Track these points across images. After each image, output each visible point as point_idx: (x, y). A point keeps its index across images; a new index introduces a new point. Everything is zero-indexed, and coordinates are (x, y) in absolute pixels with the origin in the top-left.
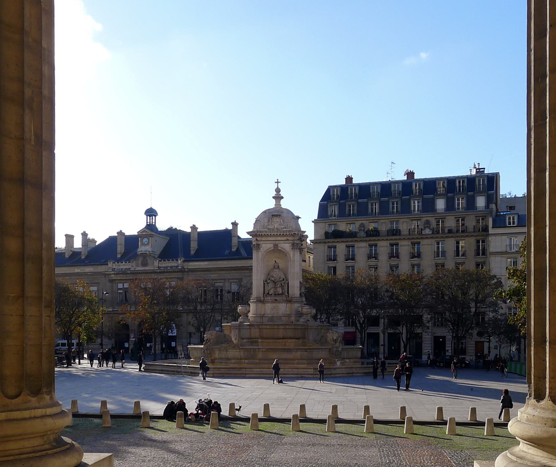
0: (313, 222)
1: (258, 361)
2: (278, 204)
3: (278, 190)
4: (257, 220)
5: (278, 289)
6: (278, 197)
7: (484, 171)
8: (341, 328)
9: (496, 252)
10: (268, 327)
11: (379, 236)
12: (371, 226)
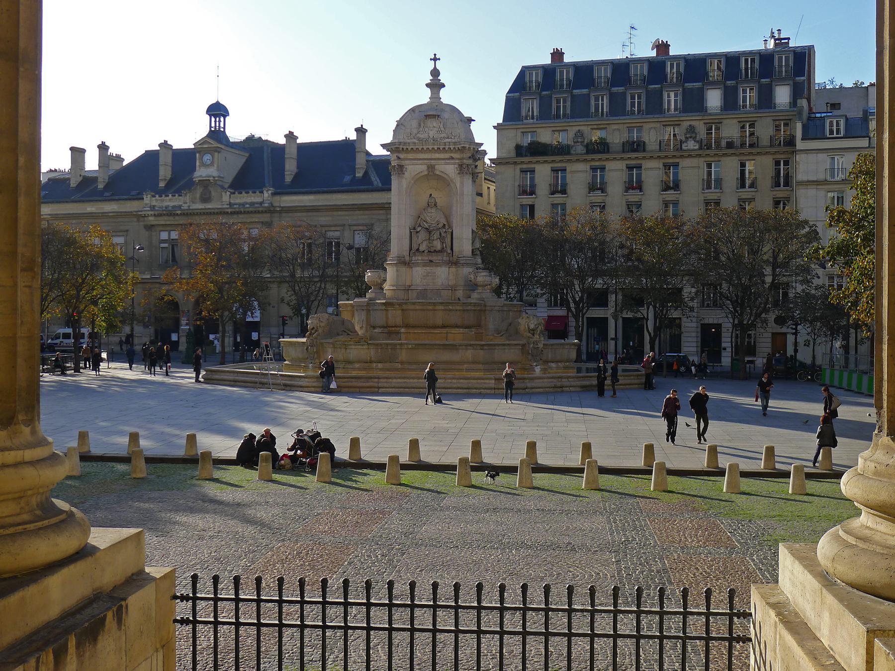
2: (435, 96)
3: (435, 73)
4: (400, 124)
5: (435, 242)
6: (436, 85)
7: (788, 43)
9: (809, 181)
10: (417, 307)
11: (608, 152)
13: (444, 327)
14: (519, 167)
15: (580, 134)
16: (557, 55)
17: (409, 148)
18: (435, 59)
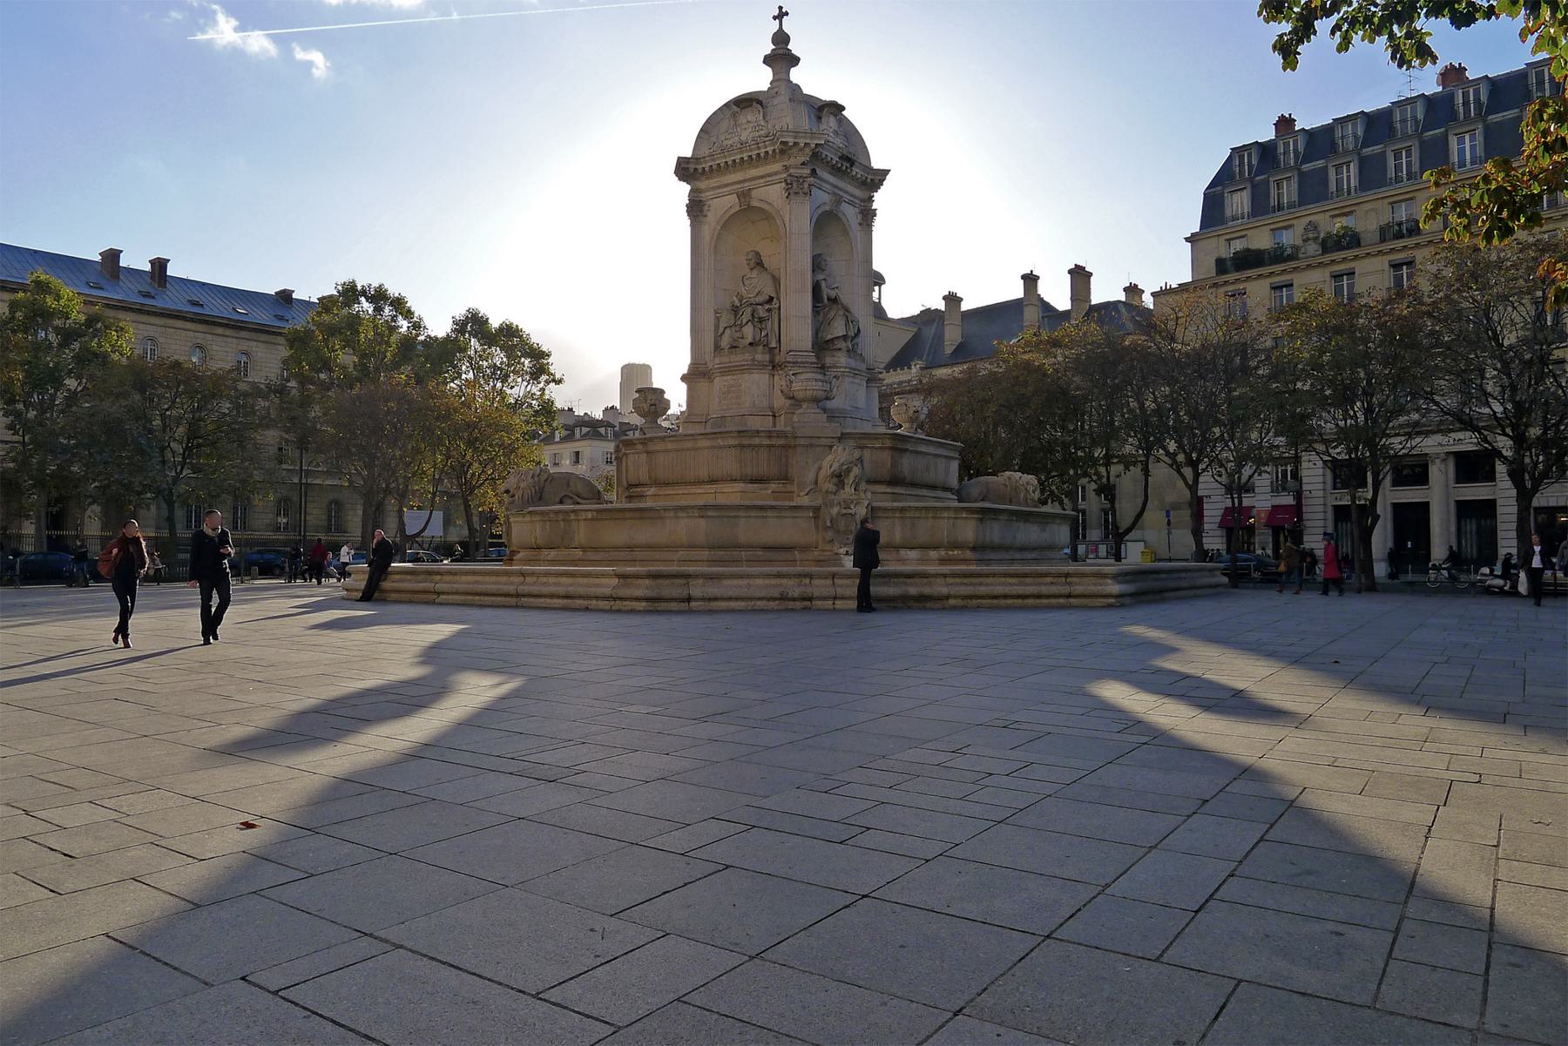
0: (1187, 239)
1: (579, 553)
2: (781, 80)
3: (781, 39)
4: (705, 131)
6: (781, 57)
8: (1263, 497)
10: (670, 446)
11: (1358, 245)
12: (1338, 225)
13: (712, 481)
14: (1222, 290)
15: (1313, 226)
16: (1285, 124)
17: (707, 166)
18: (781, 15)
